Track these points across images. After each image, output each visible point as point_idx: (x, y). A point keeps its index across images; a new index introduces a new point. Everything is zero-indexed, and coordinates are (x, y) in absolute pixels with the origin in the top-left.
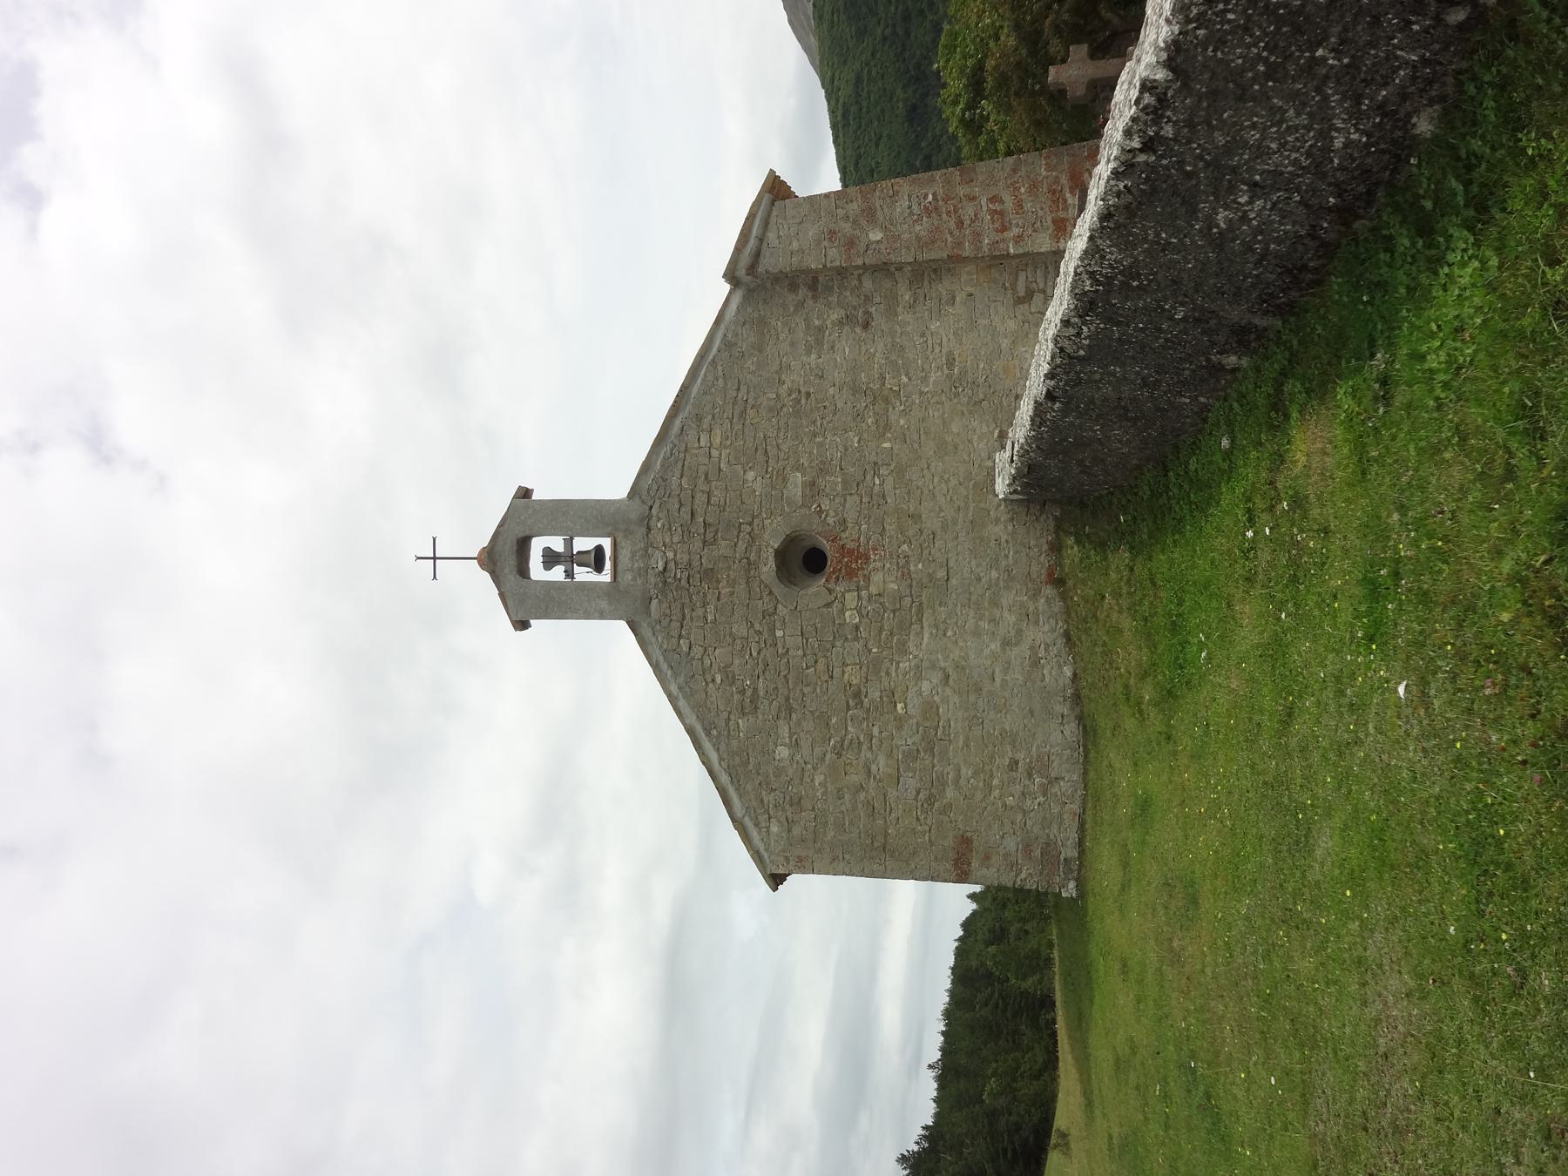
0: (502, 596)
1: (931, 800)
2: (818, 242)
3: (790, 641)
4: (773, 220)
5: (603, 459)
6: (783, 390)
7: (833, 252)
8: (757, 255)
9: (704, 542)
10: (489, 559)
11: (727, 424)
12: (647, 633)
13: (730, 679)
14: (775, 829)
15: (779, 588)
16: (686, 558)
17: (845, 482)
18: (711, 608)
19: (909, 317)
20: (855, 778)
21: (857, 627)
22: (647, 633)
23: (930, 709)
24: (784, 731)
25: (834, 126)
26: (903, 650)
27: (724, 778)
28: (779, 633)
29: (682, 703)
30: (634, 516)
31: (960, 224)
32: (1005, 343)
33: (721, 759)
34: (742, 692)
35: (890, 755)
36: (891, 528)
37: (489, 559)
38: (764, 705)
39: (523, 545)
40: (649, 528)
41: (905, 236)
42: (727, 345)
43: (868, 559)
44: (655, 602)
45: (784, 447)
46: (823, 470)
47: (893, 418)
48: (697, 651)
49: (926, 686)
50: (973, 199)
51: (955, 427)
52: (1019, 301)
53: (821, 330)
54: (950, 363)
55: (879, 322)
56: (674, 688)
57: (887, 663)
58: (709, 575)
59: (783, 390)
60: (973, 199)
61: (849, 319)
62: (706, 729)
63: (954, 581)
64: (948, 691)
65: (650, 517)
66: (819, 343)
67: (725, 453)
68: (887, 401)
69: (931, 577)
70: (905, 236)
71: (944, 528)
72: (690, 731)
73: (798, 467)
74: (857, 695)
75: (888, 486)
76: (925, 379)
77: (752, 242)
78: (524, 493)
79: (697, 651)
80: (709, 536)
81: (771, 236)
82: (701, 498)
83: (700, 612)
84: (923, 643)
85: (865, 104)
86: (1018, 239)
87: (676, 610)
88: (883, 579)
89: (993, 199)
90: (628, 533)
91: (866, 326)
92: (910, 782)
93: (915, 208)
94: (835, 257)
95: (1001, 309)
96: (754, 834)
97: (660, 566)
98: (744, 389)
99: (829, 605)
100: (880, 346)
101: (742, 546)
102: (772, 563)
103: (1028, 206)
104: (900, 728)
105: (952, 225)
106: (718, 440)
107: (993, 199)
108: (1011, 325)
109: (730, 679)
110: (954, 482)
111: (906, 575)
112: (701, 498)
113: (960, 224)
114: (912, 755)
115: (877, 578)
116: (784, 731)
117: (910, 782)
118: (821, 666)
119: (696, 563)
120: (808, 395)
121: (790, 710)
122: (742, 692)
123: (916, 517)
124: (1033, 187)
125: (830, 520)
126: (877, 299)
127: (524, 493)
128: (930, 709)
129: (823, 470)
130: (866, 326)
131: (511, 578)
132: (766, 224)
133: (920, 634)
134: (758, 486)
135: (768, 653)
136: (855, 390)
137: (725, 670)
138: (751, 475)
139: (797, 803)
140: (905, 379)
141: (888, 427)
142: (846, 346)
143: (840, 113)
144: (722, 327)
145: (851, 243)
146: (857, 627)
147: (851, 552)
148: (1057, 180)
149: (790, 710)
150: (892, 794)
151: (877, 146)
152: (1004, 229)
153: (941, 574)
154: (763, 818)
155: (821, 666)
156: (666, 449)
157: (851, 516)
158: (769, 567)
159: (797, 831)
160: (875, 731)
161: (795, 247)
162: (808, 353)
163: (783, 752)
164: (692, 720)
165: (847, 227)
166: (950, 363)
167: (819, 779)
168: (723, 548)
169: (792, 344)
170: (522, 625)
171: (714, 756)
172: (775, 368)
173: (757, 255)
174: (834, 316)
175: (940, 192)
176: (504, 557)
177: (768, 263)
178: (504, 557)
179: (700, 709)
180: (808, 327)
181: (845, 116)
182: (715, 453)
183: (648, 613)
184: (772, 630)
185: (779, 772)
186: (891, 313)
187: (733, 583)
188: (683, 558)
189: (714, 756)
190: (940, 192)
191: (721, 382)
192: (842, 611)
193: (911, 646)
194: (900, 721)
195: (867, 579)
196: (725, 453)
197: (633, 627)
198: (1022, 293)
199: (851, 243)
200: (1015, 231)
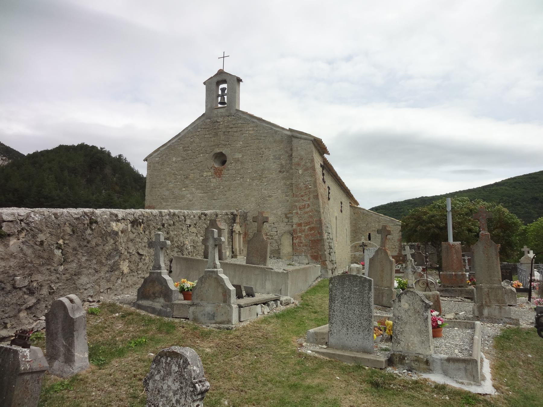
0: (212, 77)
1: (163, 199)
2: (299, 155)
3: (199, 158)
4: (306, 141)
5: (249, 102)
6: (263, 150)
7: (297, 160)
8: (297, 138)
9: (224, 132)
10: (221, 72)
11: (255, 135)
12: (202, 119)
13: (192, 143)
14: (157, 159)
15: (212, 153)
16: (220, 127)
17: (239, 169)
18: (208, 136)
19: (282, 184)
20: (168, 178)
21: (202, 176)
22: (202, 119)
23: (183, 197)
24: (179, 159)
25: (530, 174)
26: (197, 189)
27: (169, 145)
28: (201, 155)
29: (186, 131)
30: (232, 111)
31: (302, 196)
32: (275, 212)
33: (173, 143)
34: (188, 147)
35: (173, 187)
36: (227, 183)
37: (221, 72)
38: (185, 153)
39: (224, 82)
40: (228, 116)
41: (300, 180)
42: (276, 132)
43: (219, 177)
44: (209, 120)
45: (248, 152)
46: (242, 163)
47: (255, 181)
48: (198, 134)
49: (189, 195)
50: (309, 199)
51: (252, 199)
52: (286, 215)
53: (280, 159)
54: (269, 196)
55: (281, 175)
56: (189, 128)
57: (194, 185)
58: (216, 134)
59: (263, 150)
60: (309, 199)
61: (282, 166)
62: (180, 138)
63: (214, 201)
64: (187, 202)
65: (231, 116)
66: (276, 159)
67: (247, 135)
68: (260, 179)
69: (215, 195)
70: (300, 180)
71: (227, 198)
72: (179, 134)
73: (243, 156)
74: (187, 178)
75: (238, 182)
76: (265, 190)
77: (299, 136)
78: (239, 80)
79: (198, 134)
80: (226, 133)
81: (302, 141)
82: (235, 130)
83: (207, 133)
84: (199, 194)
85: (538, 184)
86: (297, 213)
87: (207, 127)
88: (214, 181)
89: (309, 205)
90: (227, 110)
91: (280, 172)
92: (167, 193)
93: (308, 183)
94: (295, 160)
95: (284, 210)
96: (156, 154)
97: (218, 121)
98: (264, 138)
99: (208, 168)
100: (274, 176)
101: (223, 142)
102: (219, 151)
103: (306, 215)
104: (179, 189)
105: (302, 194)
106: (250, 132)
107: (309, 205)
108: (280, 213)
109: (192, 143)
110: (238, 199)
111: (215, 188)
112: (235, 130)
113: (302, 196)
114: (173, 193)
115: (214, 180)
116: (179, 159)
117: (167, 193)
118: (194, 167)
119: (219, 130)
120: (262, 157)
121: (184, 160)
122: (188, 147)
123: (229, 190)
124: (311, 217)
125: (229, 166)
126: (287, 174)
127: (239, 80)
128: (183, 197)
129: (242, 163)
130: (280, 172)
131: (216, 80)
132: (305, 139)
133: (201, 193)
134: (239, 145)
135: (197, 153)
136: (263, 170)
137: (194, 141)
138: (241, 143)
139: (163, 164)
140: (265, 184)
141: (253, 180)
142: (275, 166)
143: (535, 176)
144: (281, 130)
145: (299, 165)
146: (202, 176)
147: (221, 173)
148: (313, 223)
149: (184, 160)
150: (164, 189)
151: (524, 188)
152: (300, 209)
153: (215, 198)
154: (159, 156)
155: (194, 167)
156: (248, 118)
157: (230, 172)
158: (218, 150)
159: (157, 165)
160: (179, 183)
161: (302, 150)
162: (273, 156)
163: (174, 159)
164: (182, 134)
165: (303, 163)
166: (269, 196)
167: (168, 169)
168: (223, 137)
169: (276, 151)
170: (205, 83)
171: (174, 141)
172: (270, 147)
173: (297, 138)
174: (283, 162)
175: (312, 189)
176: (221, 77)
177: (295, 141)
178: (221, 77)
179: (185, 136)
180: (281, 155)
181: (534, 177)
182: (247, 132)
183: (207, 119)
184: (202, 153)
185: (169, 158)
186: (284, 178)
187: (214, 141)
188: (221, 127)
189: (174, 141)
190: (312, 189)
191: (266, 131)
192: (206, 172)
193: (198, 191)
194: (180, 189)
195: (214, 178)
196: (247, 135)
197: (203, 115)
198: (288, 216)
199: (299, 165)
200: (299, 212)
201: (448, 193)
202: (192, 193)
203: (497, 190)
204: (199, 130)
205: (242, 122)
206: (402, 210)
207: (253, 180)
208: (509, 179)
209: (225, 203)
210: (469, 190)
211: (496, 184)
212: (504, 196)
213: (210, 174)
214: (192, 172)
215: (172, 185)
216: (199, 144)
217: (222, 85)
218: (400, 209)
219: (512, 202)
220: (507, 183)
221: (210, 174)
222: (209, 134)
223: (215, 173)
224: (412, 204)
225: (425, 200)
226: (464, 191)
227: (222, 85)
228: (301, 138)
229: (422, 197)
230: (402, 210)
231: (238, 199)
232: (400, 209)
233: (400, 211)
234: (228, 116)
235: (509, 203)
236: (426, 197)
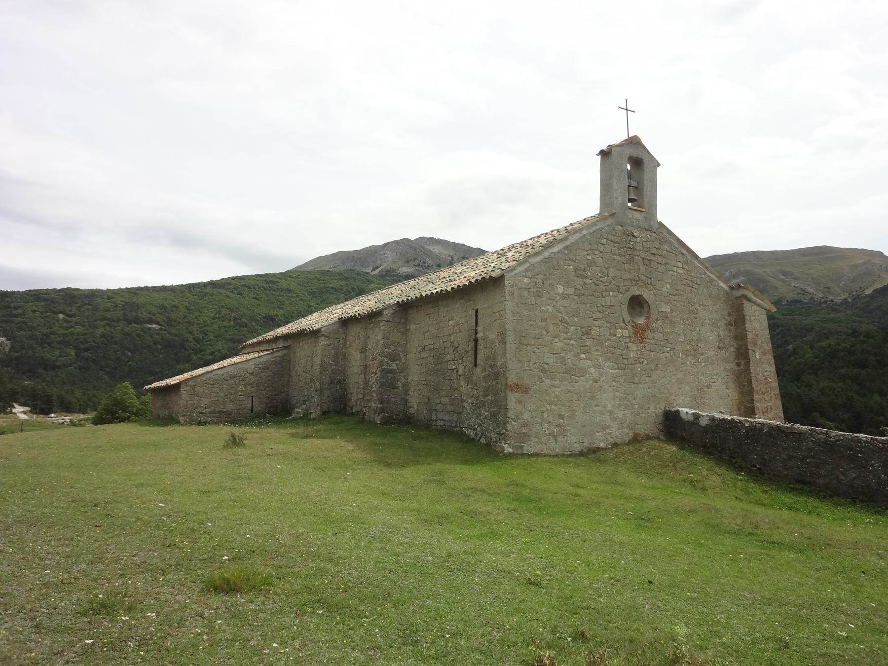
1: (544, 371)
3: (608, 299)
14: (526, 280)
19: (722, 368)
23: (584, 372)
30: (652, 223)
36: (653, 355)
38: (580, 281)
43: (641, 343)
44: (621, 228)
47: (689, 358)
48: (602, 248)
49: (592, 370)
58: (631, 259)
63: (633, 386)
64: (591, 382)
69: (635, 375)
74: (588, 334)
81: (755, 308)
82: (660, 259)
85: (277, 293)
98: (697, 286)
99: (624, 321)
102: (638, 293)
109: (592, 263)
114: (563, 361)
116: (571, 291)
117: (551, 360)
127: (605, 154)
129: (672, 323)
139: (538, 295)
146: (615, 335)
147: (643, 334)
149: (579, 296)
150: (546, 350)
151: (255, 298)
158: (636, 292)
160: (573, 342)
162: (710, 319)
163: (560, 289)
166: (708, 387)
167: (550, 308)
181: (272, 282)
192: (621, 328)
193: (608, 363)
194: (577, 355)
195: (634, 342)
201: (123, 287)
202: (598, 366)
203: (212, 295)
204: (604, 241)
205: (668, 249)
206: (19, 311)
207: (687, 356)
208: (233, 278)
209: (650, 391)
210: (163, 286)
211: (212, 284)
212: (223, 307)
213: (626, 333)
214: (596, 323)
215: (560, 344)
216: (605, 271)
217: (629, 169)
218: (16, 308)
219: (235, 319)
220: (230, 284)
221: (626, 333)
222: (620, 255)
223: (635, 333)
224: (45, 300)
225: (74, 297)
226: (153, 287)
227: (629, 169)
228: (754, 303)
229: (69, 289)
230: (19, 311)
231: (669, 387)
232: (16, 308)
233: (15, 312)
234: (647, 230)
235: (230, 321)
236: (108, 290)
